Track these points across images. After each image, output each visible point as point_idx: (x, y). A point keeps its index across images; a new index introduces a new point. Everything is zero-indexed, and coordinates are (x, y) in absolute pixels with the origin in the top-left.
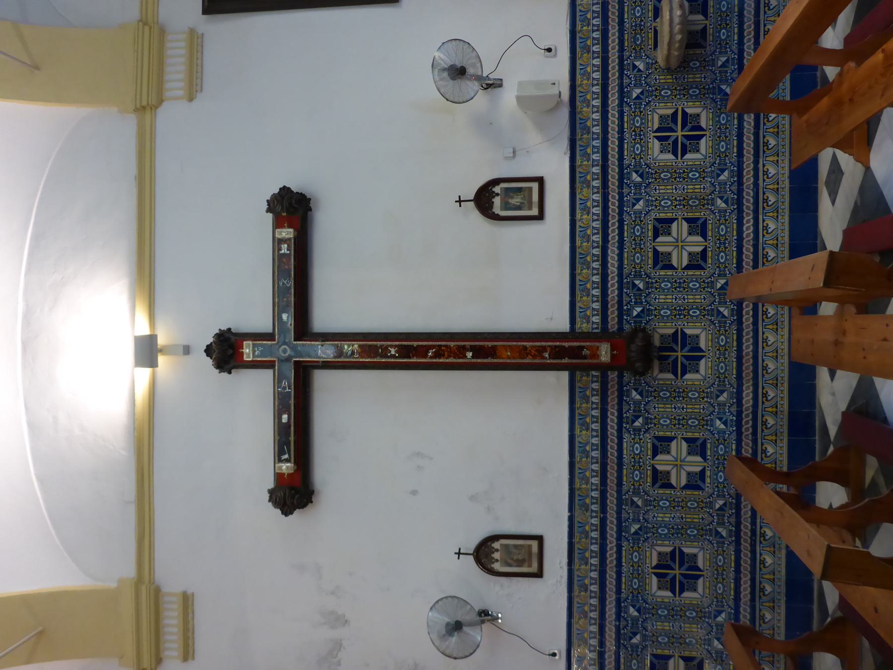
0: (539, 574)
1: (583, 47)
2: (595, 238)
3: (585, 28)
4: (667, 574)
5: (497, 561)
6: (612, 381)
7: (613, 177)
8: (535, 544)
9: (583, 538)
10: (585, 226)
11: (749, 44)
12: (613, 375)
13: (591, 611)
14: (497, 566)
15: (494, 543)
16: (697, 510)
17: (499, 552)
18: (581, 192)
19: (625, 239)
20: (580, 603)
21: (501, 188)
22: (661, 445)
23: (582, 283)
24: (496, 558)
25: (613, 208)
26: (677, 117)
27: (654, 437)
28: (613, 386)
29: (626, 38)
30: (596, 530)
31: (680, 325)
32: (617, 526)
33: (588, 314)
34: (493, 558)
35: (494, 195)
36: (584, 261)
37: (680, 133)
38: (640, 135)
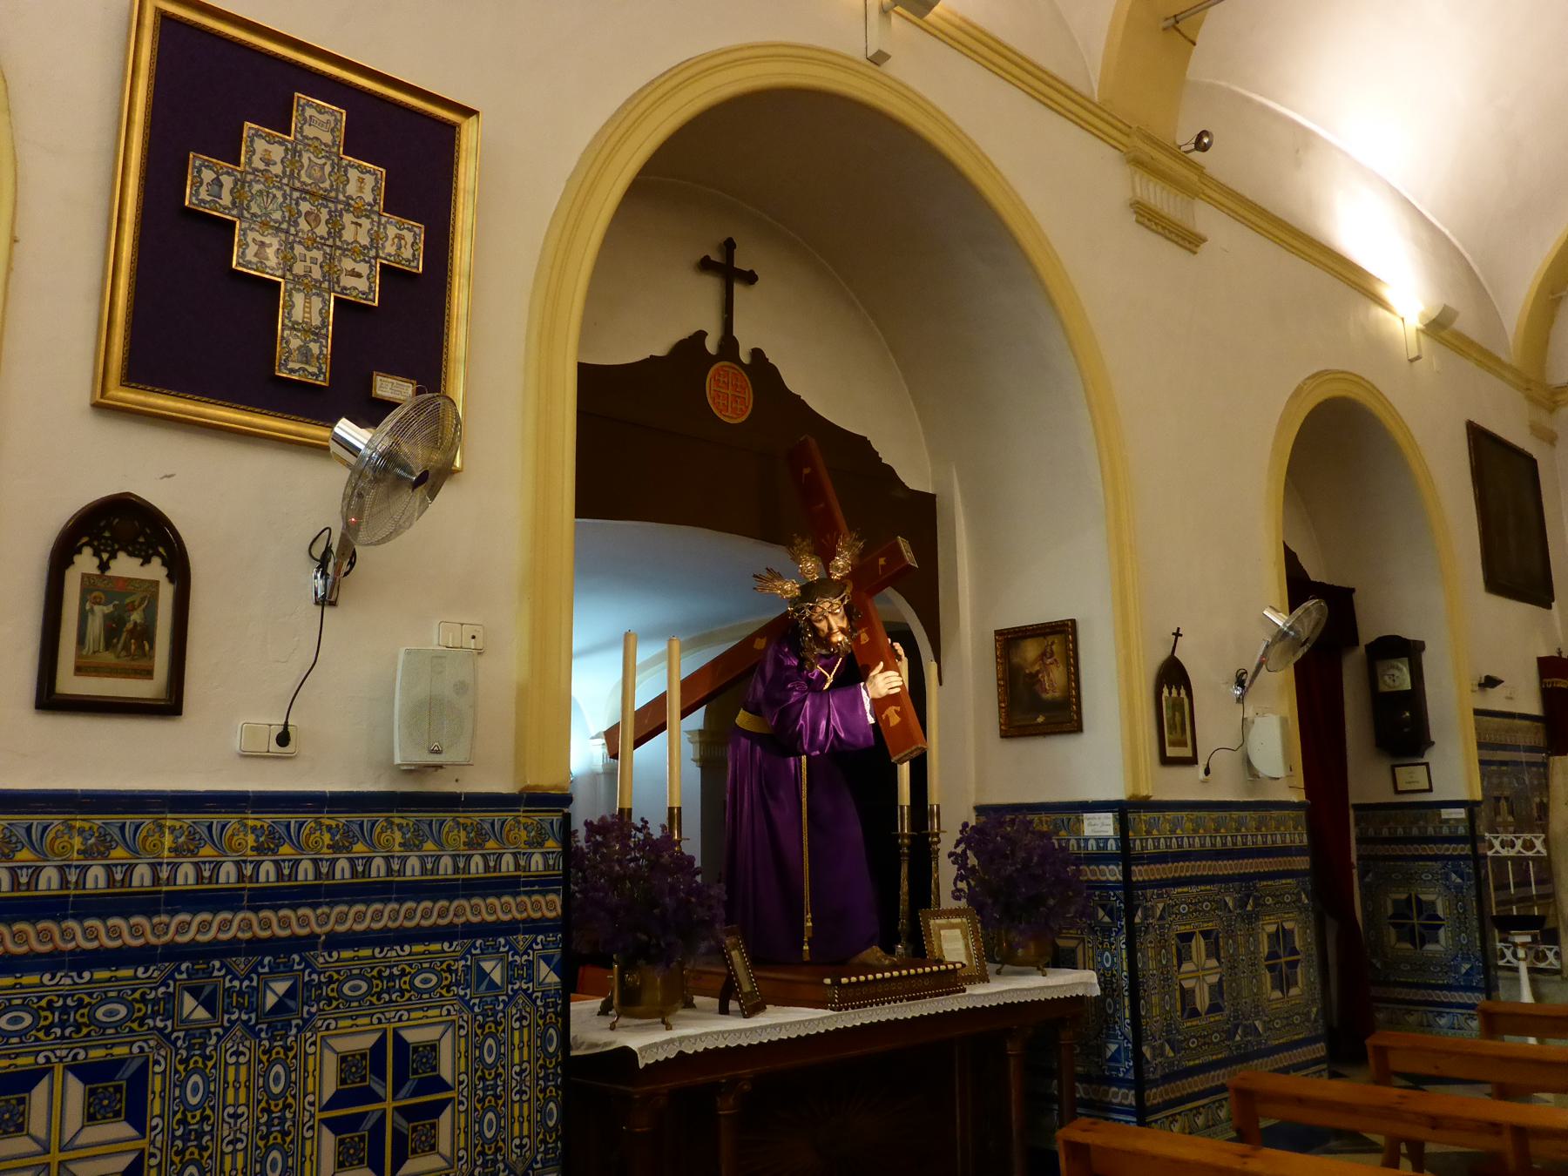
0: (49, 700)
1: (482, 828)
2: (268, 869)
3: (327, 837)
4: (382, 1076)
5: (104, 566)
6: (63, 933)
7: (204, 927)
8: (69, 683)
9: (86, 839)
10: (504, 835)
11: (1284, 1059)
12: (1465, 849)
13: (422, 859)
14: (86, 562)
15: (164, 564)
16: (478, 1141)
17: (97, 572)
18: (458, 824)
19: (407, 948)
20: (502, 826)
21: (157, 583)
22: (118, 1089)
23: (1066, 822)
24: (113, 564)
25: (78, 935)
26: (342, 1107)
27: (146, 1062)
28: (43, 936)
29: (26, 980)
30: (199, 878)
31: (312, 1116)
32: (214, 942)
33: (203, 852)
34: (113, 556)
35: (105, 556)
36: (487, 833)
37: (389, 1105)
38: (63, 1025)
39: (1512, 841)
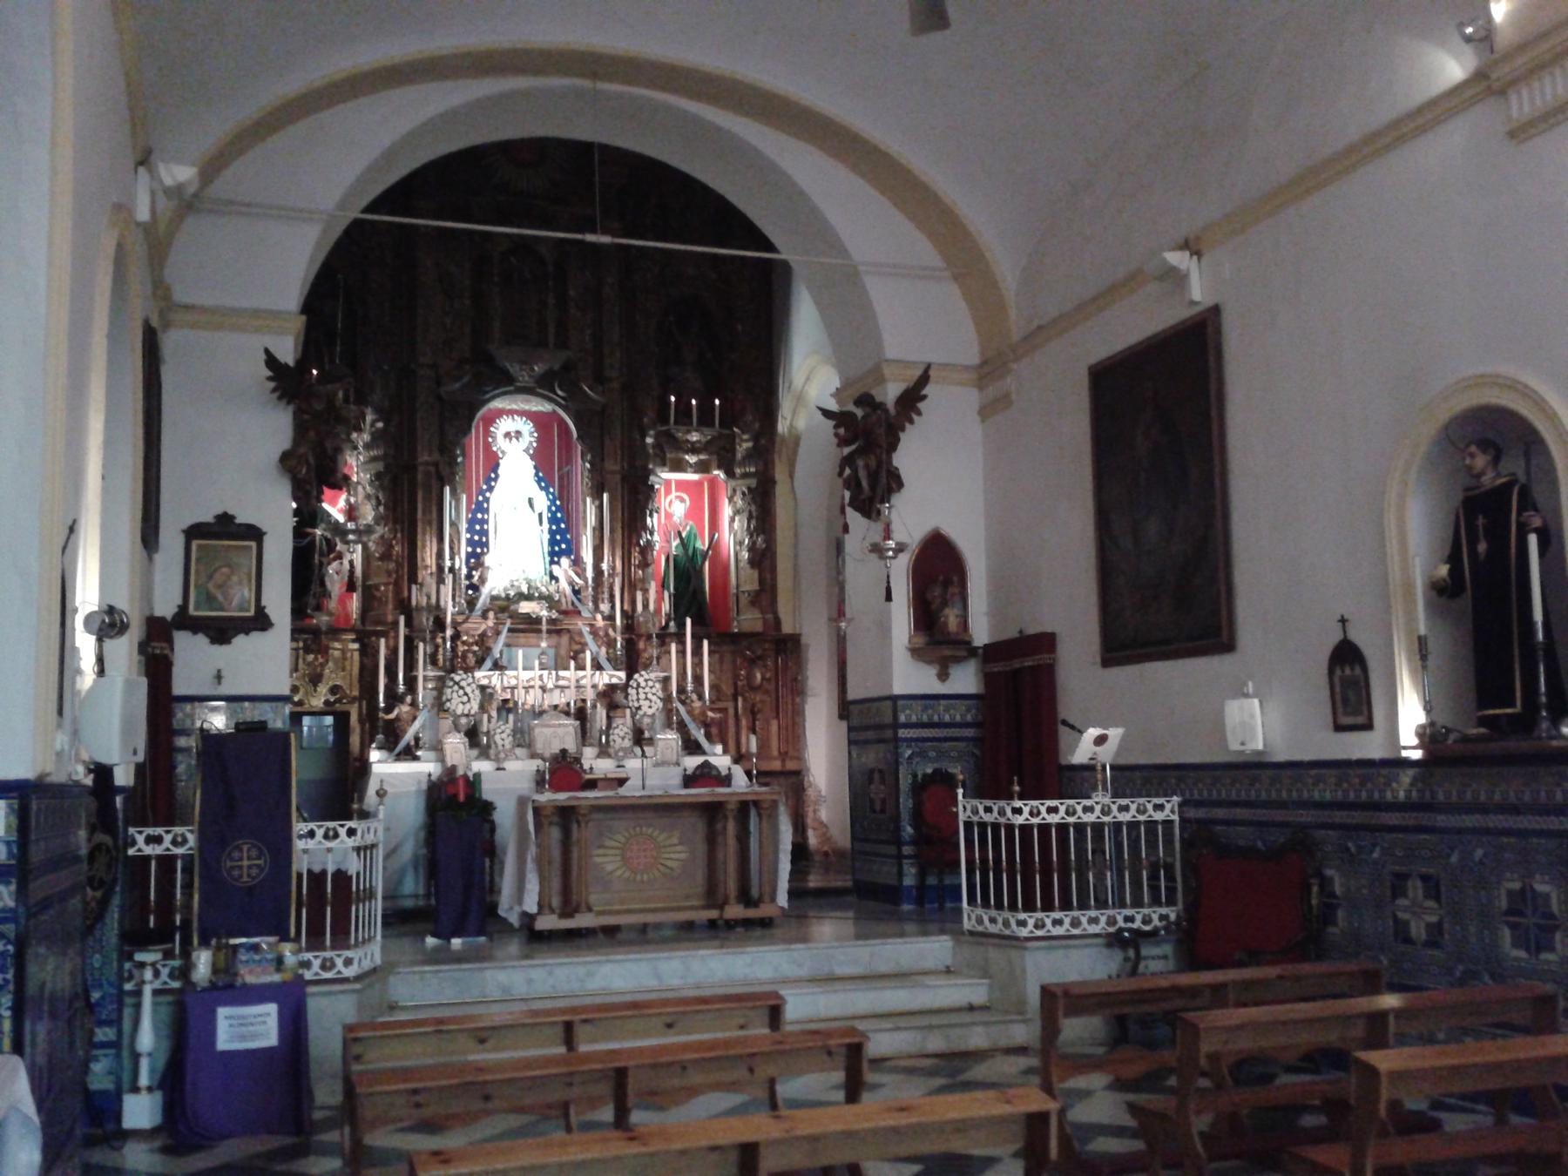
39: (1021, 808)
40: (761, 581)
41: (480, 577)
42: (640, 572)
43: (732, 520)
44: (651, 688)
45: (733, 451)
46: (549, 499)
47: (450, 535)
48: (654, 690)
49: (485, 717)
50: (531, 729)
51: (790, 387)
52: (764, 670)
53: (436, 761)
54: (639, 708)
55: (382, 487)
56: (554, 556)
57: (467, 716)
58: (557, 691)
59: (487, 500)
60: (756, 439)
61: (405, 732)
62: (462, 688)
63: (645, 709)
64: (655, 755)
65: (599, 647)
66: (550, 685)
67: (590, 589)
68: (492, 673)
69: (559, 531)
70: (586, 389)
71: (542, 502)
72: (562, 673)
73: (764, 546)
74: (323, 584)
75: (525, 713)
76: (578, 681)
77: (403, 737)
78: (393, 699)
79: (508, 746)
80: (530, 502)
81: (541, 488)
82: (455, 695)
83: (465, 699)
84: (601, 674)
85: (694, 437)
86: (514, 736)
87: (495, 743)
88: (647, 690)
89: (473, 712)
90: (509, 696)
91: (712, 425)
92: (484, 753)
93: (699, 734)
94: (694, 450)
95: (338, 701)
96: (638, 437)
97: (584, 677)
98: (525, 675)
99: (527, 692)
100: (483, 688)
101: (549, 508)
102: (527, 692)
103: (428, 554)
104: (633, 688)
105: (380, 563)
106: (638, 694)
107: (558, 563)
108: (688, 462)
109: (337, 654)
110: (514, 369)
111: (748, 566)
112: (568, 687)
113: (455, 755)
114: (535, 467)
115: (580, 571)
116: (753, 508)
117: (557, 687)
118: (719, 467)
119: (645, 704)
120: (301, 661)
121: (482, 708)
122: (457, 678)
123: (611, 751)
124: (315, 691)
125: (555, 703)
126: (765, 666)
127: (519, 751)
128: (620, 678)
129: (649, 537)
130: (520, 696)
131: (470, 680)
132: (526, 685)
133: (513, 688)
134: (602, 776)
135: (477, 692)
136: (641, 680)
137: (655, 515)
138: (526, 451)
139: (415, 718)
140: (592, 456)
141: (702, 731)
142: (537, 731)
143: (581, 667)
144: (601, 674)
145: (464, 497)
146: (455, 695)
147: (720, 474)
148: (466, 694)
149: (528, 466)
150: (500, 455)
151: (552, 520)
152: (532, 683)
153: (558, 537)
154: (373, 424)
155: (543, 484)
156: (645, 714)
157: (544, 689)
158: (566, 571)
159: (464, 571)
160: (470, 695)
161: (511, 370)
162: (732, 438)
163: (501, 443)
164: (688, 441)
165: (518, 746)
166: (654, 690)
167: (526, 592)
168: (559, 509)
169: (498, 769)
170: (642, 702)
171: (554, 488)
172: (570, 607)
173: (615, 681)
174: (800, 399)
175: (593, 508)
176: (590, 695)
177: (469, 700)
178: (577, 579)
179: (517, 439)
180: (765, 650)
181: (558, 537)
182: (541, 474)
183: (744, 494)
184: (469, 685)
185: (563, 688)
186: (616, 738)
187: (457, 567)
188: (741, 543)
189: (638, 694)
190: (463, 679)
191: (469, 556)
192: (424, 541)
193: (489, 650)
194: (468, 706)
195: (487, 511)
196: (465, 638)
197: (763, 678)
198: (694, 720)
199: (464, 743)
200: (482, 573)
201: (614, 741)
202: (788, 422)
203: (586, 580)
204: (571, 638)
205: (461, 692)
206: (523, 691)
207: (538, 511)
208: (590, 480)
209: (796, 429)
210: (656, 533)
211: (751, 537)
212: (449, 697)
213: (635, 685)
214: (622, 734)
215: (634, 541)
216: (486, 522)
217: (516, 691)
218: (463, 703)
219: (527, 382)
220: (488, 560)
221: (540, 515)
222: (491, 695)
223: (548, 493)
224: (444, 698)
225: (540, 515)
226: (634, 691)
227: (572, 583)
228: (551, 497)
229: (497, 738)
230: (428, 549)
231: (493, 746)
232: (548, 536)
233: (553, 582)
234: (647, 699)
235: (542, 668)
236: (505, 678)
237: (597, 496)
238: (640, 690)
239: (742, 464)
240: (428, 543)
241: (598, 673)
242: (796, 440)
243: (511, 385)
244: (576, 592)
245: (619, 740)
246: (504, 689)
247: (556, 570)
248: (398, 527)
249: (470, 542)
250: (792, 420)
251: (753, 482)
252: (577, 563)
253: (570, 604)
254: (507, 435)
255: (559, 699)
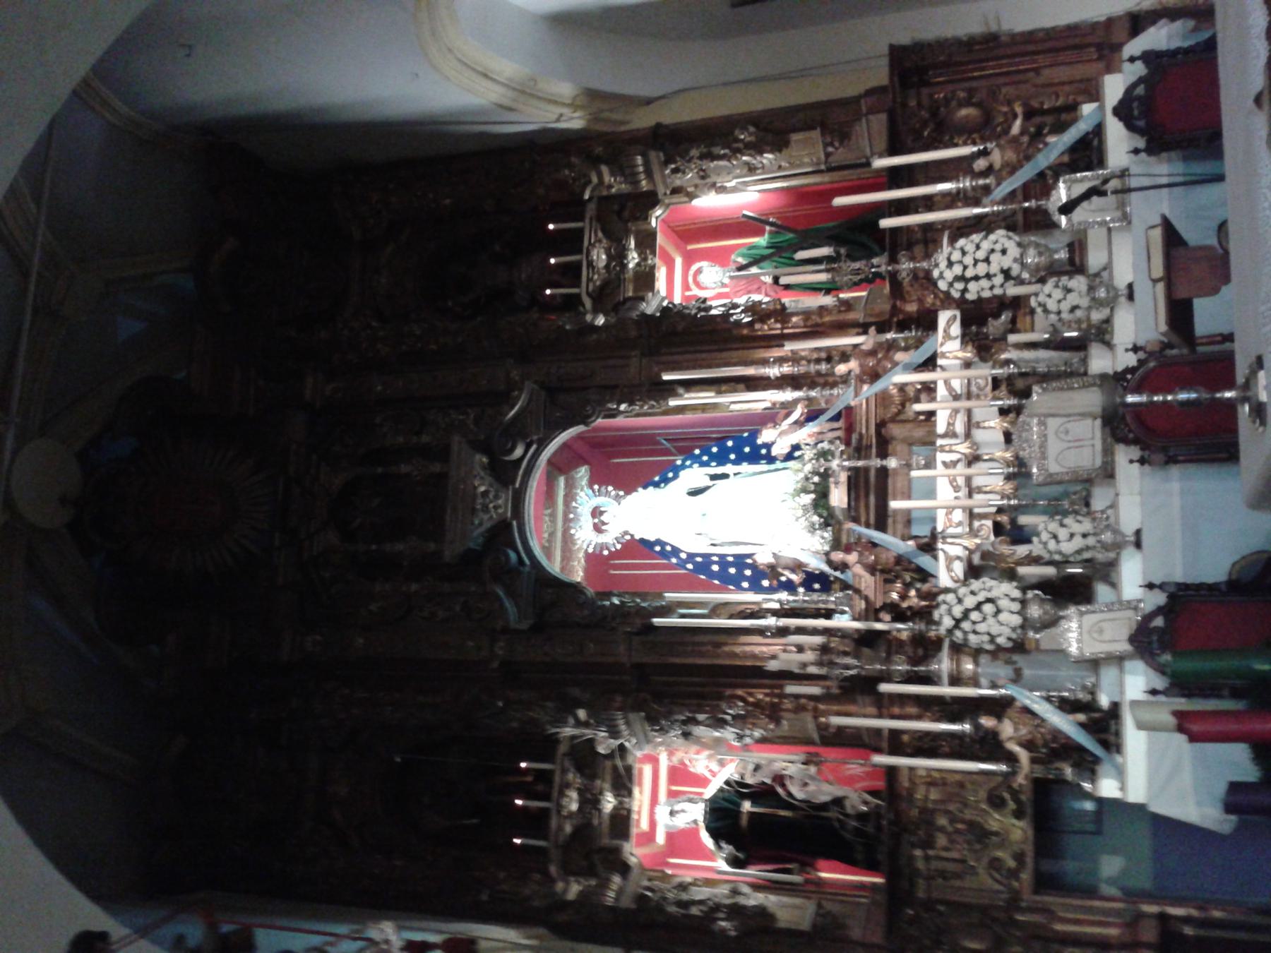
40: (809, 127)
41: (793, 570)
42: (794, 319)
43: (722, 190)
44: (964, 253)
45: (620, 197)
46: (690, 466)
47: (731, 617)
48: (970, 248)
49: (1023, 570)
50: (1051, 480)
51: (510, 109)
52: (954, 103)
53: (1122, 670)
54: (1006, 273)
55: (668, 715)
56: (759, 455)
57: (1023, 602)
58: (978, 435)
59: (691, 556)
60: (595, 161)
61: (1057, 734)
62: (966, 614)
63: (1007, 262)
64: (1103, 223)
65: (896, 364)
66: (964, 448)
67: (813, 394)
68: (941, 555)
69: (737, 449)
70: (513, 413)
71: (694, 475)
72: (941, 428)
73: (752, 129)
74: (824, 806)
75: (1021, 492)
76: (956, 397)
77: (1068, 738)
78: (988, 746)
79: (1087, 526)
80: (695, 493)
81: (676, 477)
82: (981, 628)
83: (988, 608)
84: (943, 355)
85: (600, 257)
86: (1065, 514)
87: (1079, 552)
88: (968, 260)
89: (1017, 594)
90: (989, 523)
91: (580, 232)
92: (1106, 571)
93: (1058, 144)
94: (618, 257)
95: (1015, 794)
96: (595, 336)
97: (947, 382)
98: (945, 494)
99: (980, 490)
100: (973, 572)
101: (703, 464)
102: (980, 490)
103: (764, 649)
104: (965, 290)
105: (785, 722)
106: (976, 278)
107: (768, 446)
108: (638, 264)
109: (934, 795)
110: (485, 521)
111: (785, 152)
112: (969, 412)
113: (1107, 635)
114: (645, 487)
115: (784, 412)
116: (694, 152)
117: (968, 435)
118: (646, 218)
119: (998, 262)
120: (944, 854)
121: (1010, 575)
122: (948, 622)
123: (1097, 316)
124: (996, 834)
125: (1002, 438)
126: (947, 101)
127: (1099, 501)
128: (950, 323)
129: (739, 310)
130: (987, 502)
131: (950, 597)
132: (963, 492)
133: (972, 516)
134: (1160, 287)
135: (975, 584)
136: (949, 275)
137: (709, 303)
138: (617, 498)
139: (1027, 711)
140: (611, 401)
141: (1052, 139)
142: (1054, 468)
143: (929, 389)
144: (943, 355)
145: (670, 596)
146: (981, 628)
147: (657, 217)
148: (978, 607)
149: (643, 497)
150: (628, 537)
151: (722, 459)
152: (961, 481)
153: (747, 450)
154: (579, 724)
155: (670, 475)
156: (1020, 261)
157: (973, 459)
158: (781, 434)
159: (784, 596)
160: (981, 597)
161: (487, 525)
162: (605, 201)
163: (610, 538)
164: (607, 267)
165: (1087, 505)
166: (970, 248)
167: (813, 496)
168: (706, 451)
169: (1138, 545)
170: (994, 268)
171: (676, 460)
172: (840, 424)
173: (956, 329)
174: (525, 91)
175: (686, 396)
176: (984, 372)
177: (989, 600)
178: (796, 415)
179: (602, 513)
180: (919, 105)
181: (747, 450)
182: (657, 479)
183: (675, 171)
184: (960, 601)
185: (971, 425)
186: (1065, 306)
187: (777, 606)
188: (752, 169)
189: (976, 278)
190: (949, 612)
191: (756, 587)
192: (746, 656)
193: (899, 559)
194: (1004, 603)
195: (706, 556)
196: (895, 596)
197: (967, 103)
198: (1028, 158)
199: (1082, 614)
200: (785, 568)
201: (1074, 309)
202: (565, 111)
203: (795, 402)
204: (894, 419)
205: (975, 616)
206: (978, 497)
207: (709, 482)
208: (645, 403)
209: (575, 98)
210: (736, 300)
211: (739, 151)
212: (986, 638)
213: (959, 286)
214: (1058, 294)
215: (745, 332)
216: (722, 557)
217: (976, 510)
218: (998, 611)
219: (507, 500)
220: (764, 558)
221: (714, 477)
222: (985, 555)
223: (683, 467)
224: (989, 647)
225: (714, 477)
226: (972, 286)
227: (799, 424)
228: (688, 463)
229: (1068, 547)
230: (757, 650)
231: (1087, 555)
232: (745, 464)
233: (797, 454)
234: (987, 260)
235: (930, 464)
236: (951, 531)
237: (670, 389)
238: (969, 273)
239: (632, 179)
240: (748, 649)
241: (940, 362)
242: (593, 96)
243: (509, 526)
244: (811, 417)
245: (1073, 299)
246: (973, 533)
247: (779, 449)
248: (728, 692)
249: (736, 582)
250: (564, 104)
251: (656, 157)
252: (771, 417)
253: (836, 425)
254: (598, 528)
255: (992, 428)
